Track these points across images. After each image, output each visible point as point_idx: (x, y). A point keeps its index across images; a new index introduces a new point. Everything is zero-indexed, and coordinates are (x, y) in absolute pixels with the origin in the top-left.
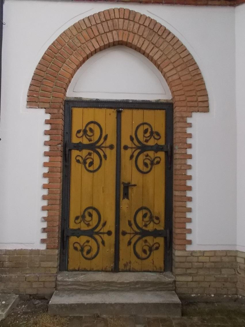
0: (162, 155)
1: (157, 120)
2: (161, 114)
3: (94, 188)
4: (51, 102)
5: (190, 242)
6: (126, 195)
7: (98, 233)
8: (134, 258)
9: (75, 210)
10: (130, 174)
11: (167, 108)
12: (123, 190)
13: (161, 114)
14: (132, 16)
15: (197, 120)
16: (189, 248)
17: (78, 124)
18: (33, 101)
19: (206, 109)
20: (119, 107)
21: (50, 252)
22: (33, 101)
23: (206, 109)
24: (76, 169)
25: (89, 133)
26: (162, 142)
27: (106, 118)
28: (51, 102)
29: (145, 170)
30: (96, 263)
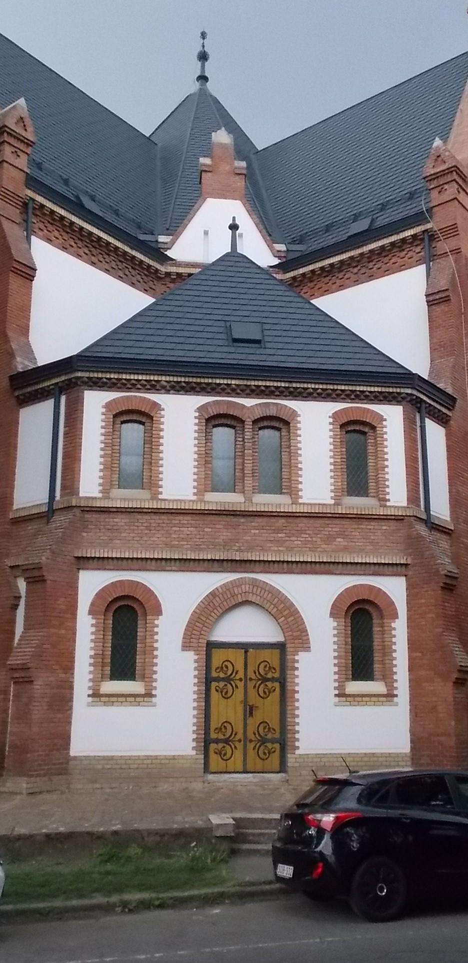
0: (277, 746)
1: (273, 657)
2: (277, 652)
3: (228, 711)
4: (248, 426)
5: (298, 748)
6: (251, 714)
7: (232, 741)
8: (259, 761)
9: (213, 725)
10: (253, 698)
11: (281, 647)
12: (250, 710)
13: (277, 652)
14: (255, 583)
15: (301, 656)
16: (297, 752)
17: (216, 661)
18: (186, 647)
19: (307, 649)
20: (245, 647)
21: (198, 757)
22: (186, 647)
23: (307, 649)
24: (215, 696)
25: (225, 669)
26: (277, 735)
27: (237, 658)
28: (248, 426)
29: (265, 757)
30: (231, 765)
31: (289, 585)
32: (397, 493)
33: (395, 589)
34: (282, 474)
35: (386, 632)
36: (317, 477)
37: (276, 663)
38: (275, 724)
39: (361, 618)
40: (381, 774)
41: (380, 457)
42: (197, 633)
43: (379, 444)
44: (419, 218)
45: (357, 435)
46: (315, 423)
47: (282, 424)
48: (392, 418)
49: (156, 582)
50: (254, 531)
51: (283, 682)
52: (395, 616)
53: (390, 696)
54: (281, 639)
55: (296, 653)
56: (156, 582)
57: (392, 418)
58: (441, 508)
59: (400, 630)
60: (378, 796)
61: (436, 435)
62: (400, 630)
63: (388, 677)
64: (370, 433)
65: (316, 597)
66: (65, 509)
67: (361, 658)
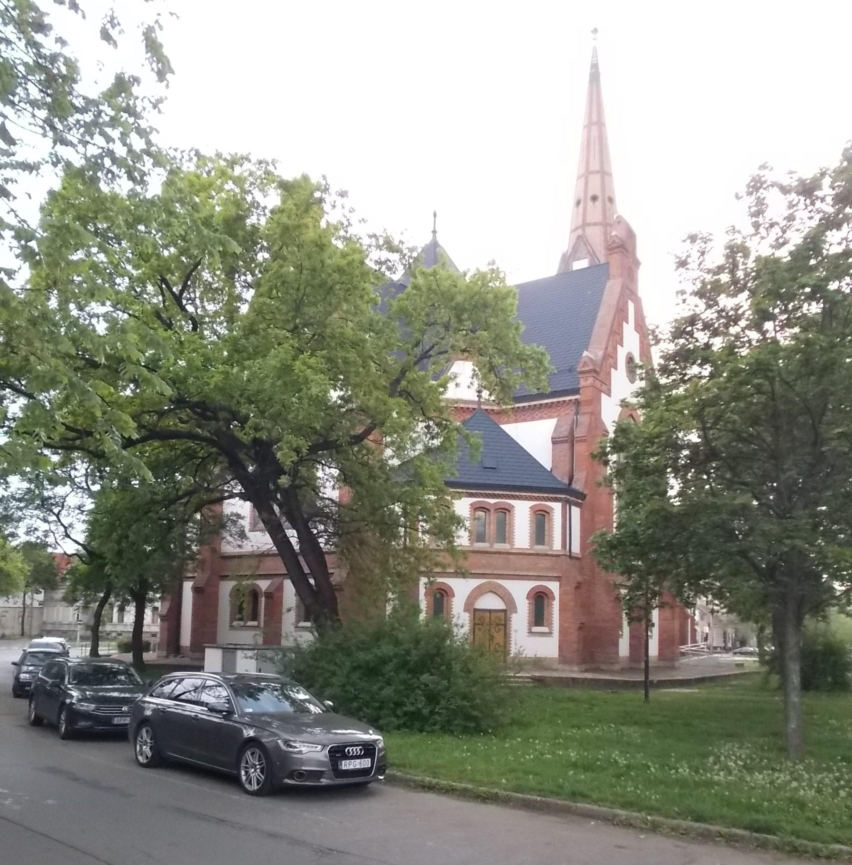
11: (504, 611)
15: (514, 616)
19: (516, 612)
23: (516, 612)
31: (507, 584)
32: (557, 545)
33: (554, 587)
34: (504, 532)
35: (550, 605)
36: (522, 535)
37: (503, 618)
38: (502, 644)
39: (539, 599)
40: (47, 645)
41: (551, 528)
42: (469, 606)
43: (551, 520)
44: (576, 391)
45: (541, 519)
46: (522, 511)
47: (506, 511)
48: (557, 507)
49: (454, 583)
50: (495, 559)
51: (505, 625)
52: (554, 599)
53: (550, 634)
54: (505, 608)
55: (32, 275)
56: (454, 583)
57: (557, 507)
58: (576, 549)
59: (556, 605)
60: (537, 674)
61: (576, 512)
62: (556, 605)
63: (550, 625)
64: (547, 515)
65: (520, 590)
66: (422, 555)
67: (539, 616)
